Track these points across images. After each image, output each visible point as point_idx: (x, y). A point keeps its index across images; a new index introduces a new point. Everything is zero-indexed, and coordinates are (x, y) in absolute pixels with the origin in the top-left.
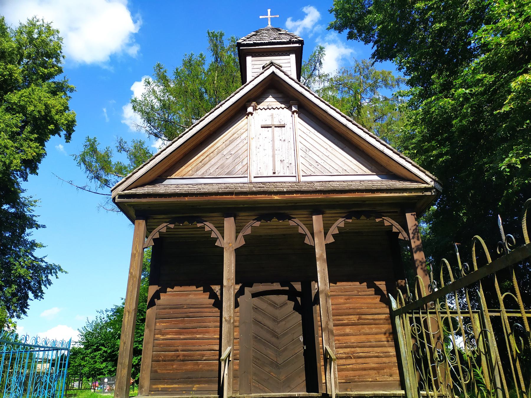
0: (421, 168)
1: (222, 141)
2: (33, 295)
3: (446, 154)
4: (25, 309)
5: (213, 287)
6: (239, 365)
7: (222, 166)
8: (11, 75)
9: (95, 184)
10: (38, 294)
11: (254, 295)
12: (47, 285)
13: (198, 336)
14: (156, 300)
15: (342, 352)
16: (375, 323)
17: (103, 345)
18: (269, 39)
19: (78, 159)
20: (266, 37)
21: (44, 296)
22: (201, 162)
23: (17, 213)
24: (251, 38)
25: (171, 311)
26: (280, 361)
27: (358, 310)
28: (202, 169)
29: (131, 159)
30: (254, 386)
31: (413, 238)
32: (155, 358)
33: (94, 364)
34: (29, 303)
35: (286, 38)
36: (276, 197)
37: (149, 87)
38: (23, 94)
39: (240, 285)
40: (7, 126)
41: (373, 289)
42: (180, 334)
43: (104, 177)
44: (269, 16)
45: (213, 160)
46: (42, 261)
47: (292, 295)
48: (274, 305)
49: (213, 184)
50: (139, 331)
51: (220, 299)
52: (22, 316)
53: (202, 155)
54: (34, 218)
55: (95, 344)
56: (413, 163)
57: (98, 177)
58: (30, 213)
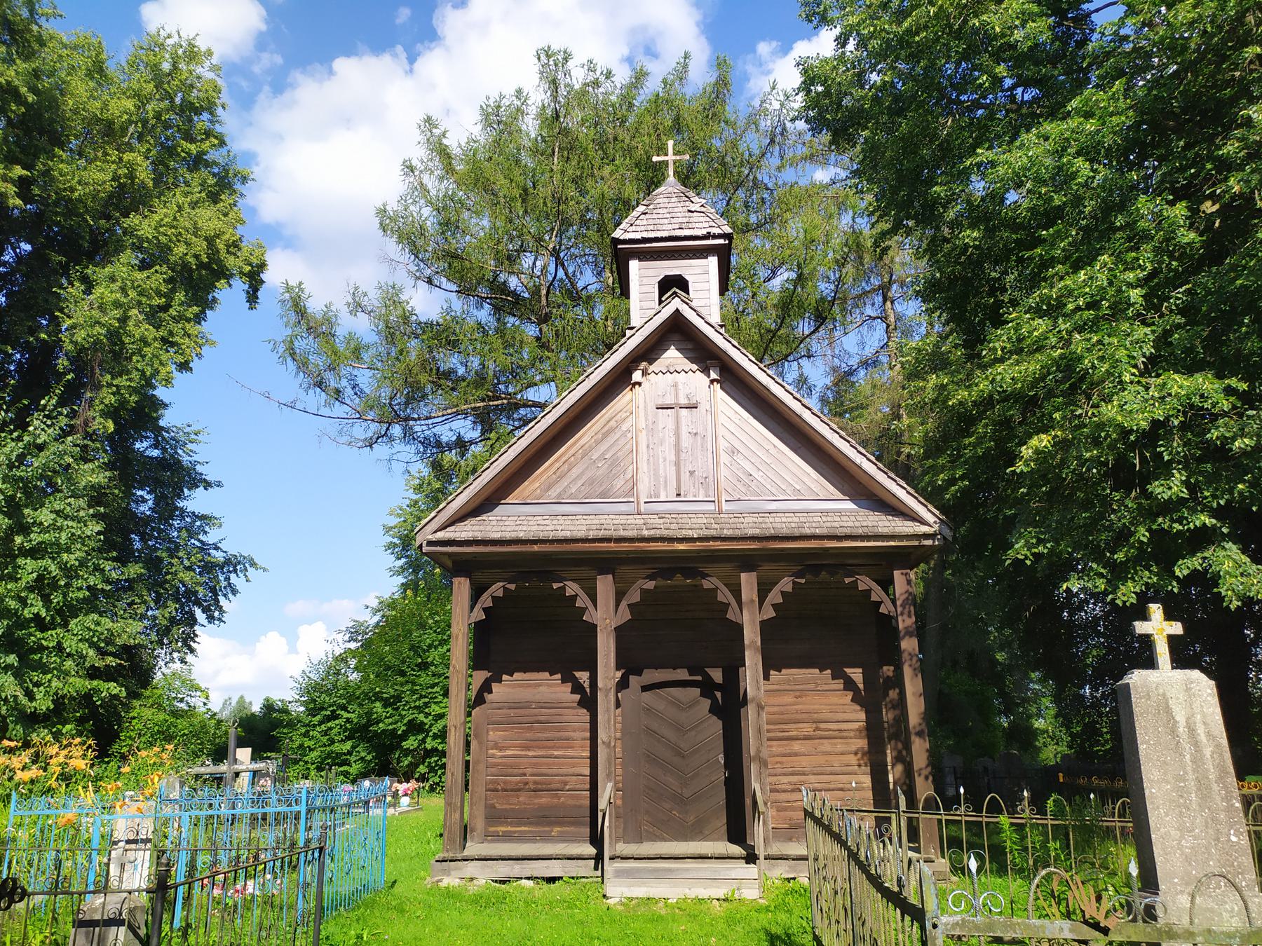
0: (920, 499)
1: (591, 433)
2: (205, 616)
3: (962, 478)
4: (192, 643)
5: (578, 674)
6: (623, 798)
7: (591, 482)
8: (131, 176)
9: (315, 398)
10: (214, 612)
11: (645, 688)
12: (230, 595)
13: (556, 753)
14: (485, 694)
15: (786, 781)
16: (841, 736)
17: (344, 708)
18: (670, 227)
19: (281, 350)
20: (666, 221)
21: (226, 617)
22: (554, 473)
23: (164, 459)
24: (637, 222)
25: (512, 712)
26: (687, 793)
27: (816, 715)
28: (557, 485)
29: (378, 333)
30: (647, 831)
31: (902, 614)
32: (491, 786)
33: (329, 745)
34: (197, 632)
35: (701, 225)
36: (681, 547)
37: (411, 180)
38: (162, 220)
39: (623, 671)
40: (140, 294)
41: (842, 681)
42: (528, 748)
43: (333, 384)
44: (671, 157)
45: (574, 470)
46: (217, 548)
47: (707, 688)
48: (677, 704)
49: (578, 517)
50: (418, 688)
51: (588, 690)
52: (189, 658)
53: (556, 461)
54: (199, 468)
55: (330, 706)
56: (909, 488)
57: (320, 384)
58: (189, 458)
